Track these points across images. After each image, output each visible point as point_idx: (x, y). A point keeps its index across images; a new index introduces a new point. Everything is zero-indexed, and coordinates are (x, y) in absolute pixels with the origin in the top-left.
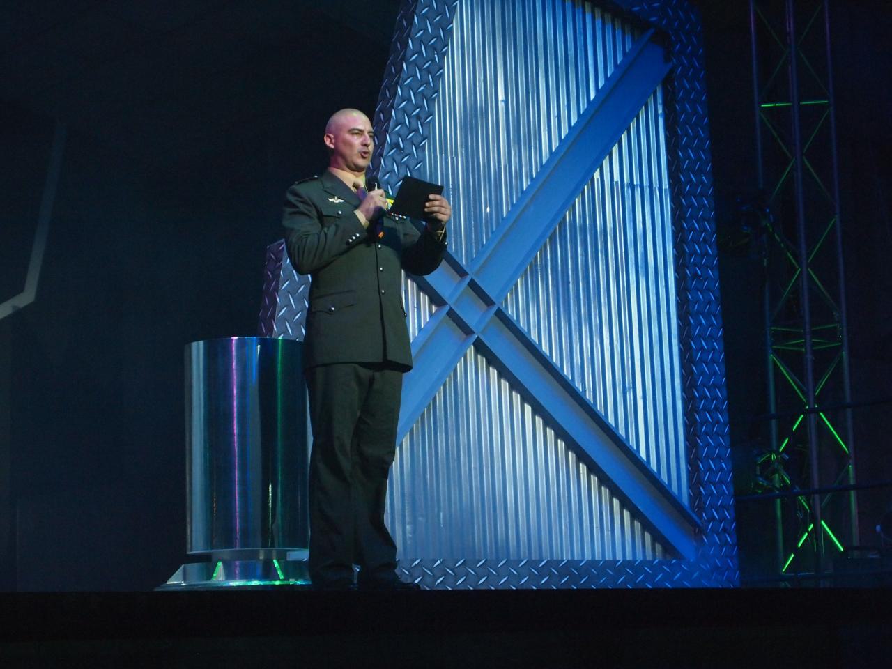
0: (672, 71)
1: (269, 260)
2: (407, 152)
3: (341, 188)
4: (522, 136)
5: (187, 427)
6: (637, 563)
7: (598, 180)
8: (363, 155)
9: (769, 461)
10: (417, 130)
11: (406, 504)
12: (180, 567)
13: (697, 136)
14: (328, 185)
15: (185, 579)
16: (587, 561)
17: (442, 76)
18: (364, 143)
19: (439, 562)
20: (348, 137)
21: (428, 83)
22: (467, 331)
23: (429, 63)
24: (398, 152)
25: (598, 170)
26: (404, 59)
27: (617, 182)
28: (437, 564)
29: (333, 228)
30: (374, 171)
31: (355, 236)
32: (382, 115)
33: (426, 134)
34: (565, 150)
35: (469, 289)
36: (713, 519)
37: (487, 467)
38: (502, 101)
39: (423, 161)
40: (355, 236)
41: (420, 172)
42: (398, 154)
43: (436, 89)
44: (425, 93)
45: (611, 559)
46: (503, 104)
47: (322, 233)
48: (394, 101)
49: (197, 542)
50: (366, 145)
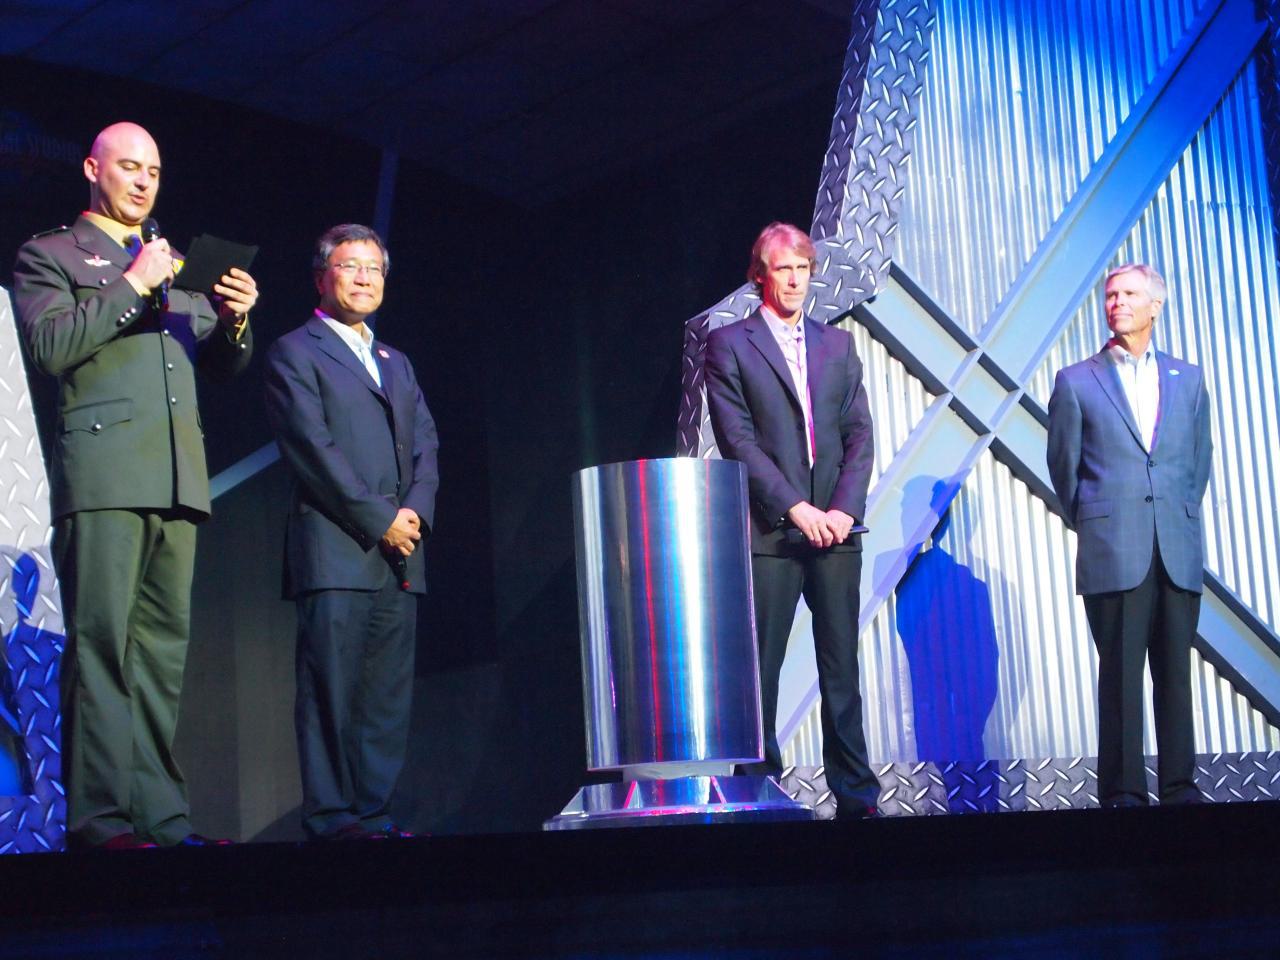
0: (1269, 33)
1: (688, 342)
2: (881, 175)
3: (100, 244)
5: (580, 590)
6: (1243, 756)
7: (1163, 199)
8: (137, 200)
10: (893, 143)
11: (901, 684)
12: (578, 791)
14: (84, 239)
15: (586, 807)
16: (1276, 753)
17: (927, 61)
18: (139, 183)
19: (952, 765)
20: (117, 170)
21: (907, 73)
22: (980, 429)
23: (909, 43)
24: (869, 176)
25: (1164, 184)
27: (1192, 202)
28: (949, 769)
29: (94, 303)
30: (834, 204)
31: (129, 311)
32: (842, 123)
33: (908, 147)
34: (1112, 159)
35: (980, 366)
37: (1017, 625)
38: (1018, 92)
40: (129, 311)
41: (901, 203)
42: (870, 179)
43: (920, 81)
44: (904, 88)
45: (1205, 752)
46: (1019, 97)
47: (79, 310)
48: (859, 101)
49: (604, 752)
50: (141, 188)
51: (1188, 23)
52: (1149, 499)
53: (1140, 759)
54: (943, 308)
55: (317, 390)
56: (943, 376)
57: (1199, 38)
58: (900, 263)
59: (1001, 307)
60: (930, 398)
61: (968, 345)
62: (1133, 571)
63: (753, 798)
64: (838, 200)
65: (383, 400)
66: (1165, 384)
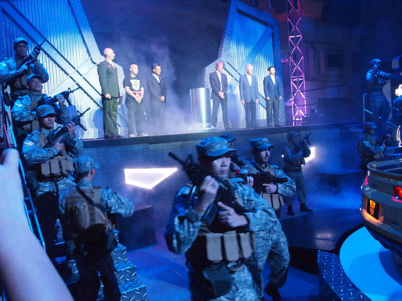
4: (287, 190)
9: (291, 100)
10: (228, 47)
13: (277, 31)
26: (225, 34)
36: (281, 111)
39: (229, 52)
51: (262, 33)
52: (251, 92)
53: (105, 140)
54: (234, 67)
55: (151, 83)
56: (233, 75)
57: (264, 34)
58: (229, 61)
59: (240, 67)
60: (232, 78)
61: (237, 71)
62: (249, 101)
63: (210, 127)
64: (221, 54)
65: (160, 84)
66: (252, 78)
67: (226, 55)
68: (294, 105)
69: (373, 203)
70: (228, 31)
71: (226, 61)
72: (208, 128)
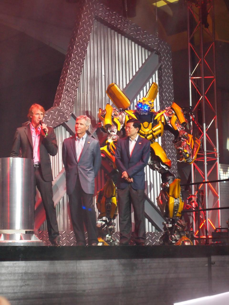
10: (74, 85)
58: (74, 113)
64: (61, 97)
67: (70, 101)
68: (197, 207)
69: (36, 159)
70: (77, 47)
71: (68, 112)
72: (25, 239)
